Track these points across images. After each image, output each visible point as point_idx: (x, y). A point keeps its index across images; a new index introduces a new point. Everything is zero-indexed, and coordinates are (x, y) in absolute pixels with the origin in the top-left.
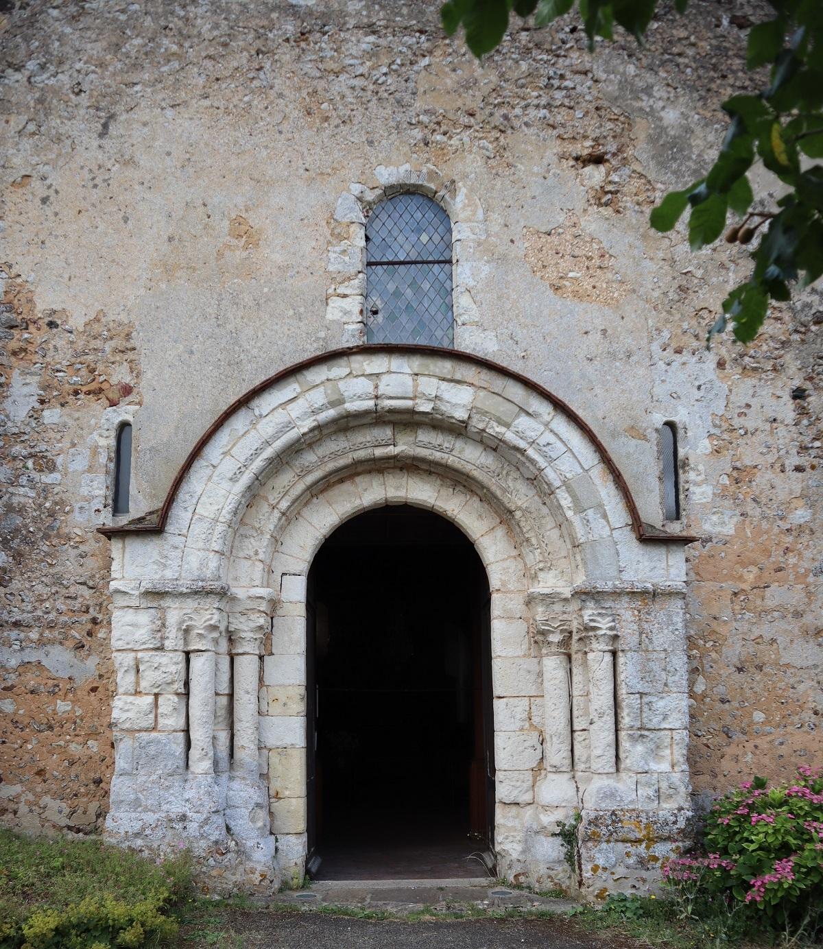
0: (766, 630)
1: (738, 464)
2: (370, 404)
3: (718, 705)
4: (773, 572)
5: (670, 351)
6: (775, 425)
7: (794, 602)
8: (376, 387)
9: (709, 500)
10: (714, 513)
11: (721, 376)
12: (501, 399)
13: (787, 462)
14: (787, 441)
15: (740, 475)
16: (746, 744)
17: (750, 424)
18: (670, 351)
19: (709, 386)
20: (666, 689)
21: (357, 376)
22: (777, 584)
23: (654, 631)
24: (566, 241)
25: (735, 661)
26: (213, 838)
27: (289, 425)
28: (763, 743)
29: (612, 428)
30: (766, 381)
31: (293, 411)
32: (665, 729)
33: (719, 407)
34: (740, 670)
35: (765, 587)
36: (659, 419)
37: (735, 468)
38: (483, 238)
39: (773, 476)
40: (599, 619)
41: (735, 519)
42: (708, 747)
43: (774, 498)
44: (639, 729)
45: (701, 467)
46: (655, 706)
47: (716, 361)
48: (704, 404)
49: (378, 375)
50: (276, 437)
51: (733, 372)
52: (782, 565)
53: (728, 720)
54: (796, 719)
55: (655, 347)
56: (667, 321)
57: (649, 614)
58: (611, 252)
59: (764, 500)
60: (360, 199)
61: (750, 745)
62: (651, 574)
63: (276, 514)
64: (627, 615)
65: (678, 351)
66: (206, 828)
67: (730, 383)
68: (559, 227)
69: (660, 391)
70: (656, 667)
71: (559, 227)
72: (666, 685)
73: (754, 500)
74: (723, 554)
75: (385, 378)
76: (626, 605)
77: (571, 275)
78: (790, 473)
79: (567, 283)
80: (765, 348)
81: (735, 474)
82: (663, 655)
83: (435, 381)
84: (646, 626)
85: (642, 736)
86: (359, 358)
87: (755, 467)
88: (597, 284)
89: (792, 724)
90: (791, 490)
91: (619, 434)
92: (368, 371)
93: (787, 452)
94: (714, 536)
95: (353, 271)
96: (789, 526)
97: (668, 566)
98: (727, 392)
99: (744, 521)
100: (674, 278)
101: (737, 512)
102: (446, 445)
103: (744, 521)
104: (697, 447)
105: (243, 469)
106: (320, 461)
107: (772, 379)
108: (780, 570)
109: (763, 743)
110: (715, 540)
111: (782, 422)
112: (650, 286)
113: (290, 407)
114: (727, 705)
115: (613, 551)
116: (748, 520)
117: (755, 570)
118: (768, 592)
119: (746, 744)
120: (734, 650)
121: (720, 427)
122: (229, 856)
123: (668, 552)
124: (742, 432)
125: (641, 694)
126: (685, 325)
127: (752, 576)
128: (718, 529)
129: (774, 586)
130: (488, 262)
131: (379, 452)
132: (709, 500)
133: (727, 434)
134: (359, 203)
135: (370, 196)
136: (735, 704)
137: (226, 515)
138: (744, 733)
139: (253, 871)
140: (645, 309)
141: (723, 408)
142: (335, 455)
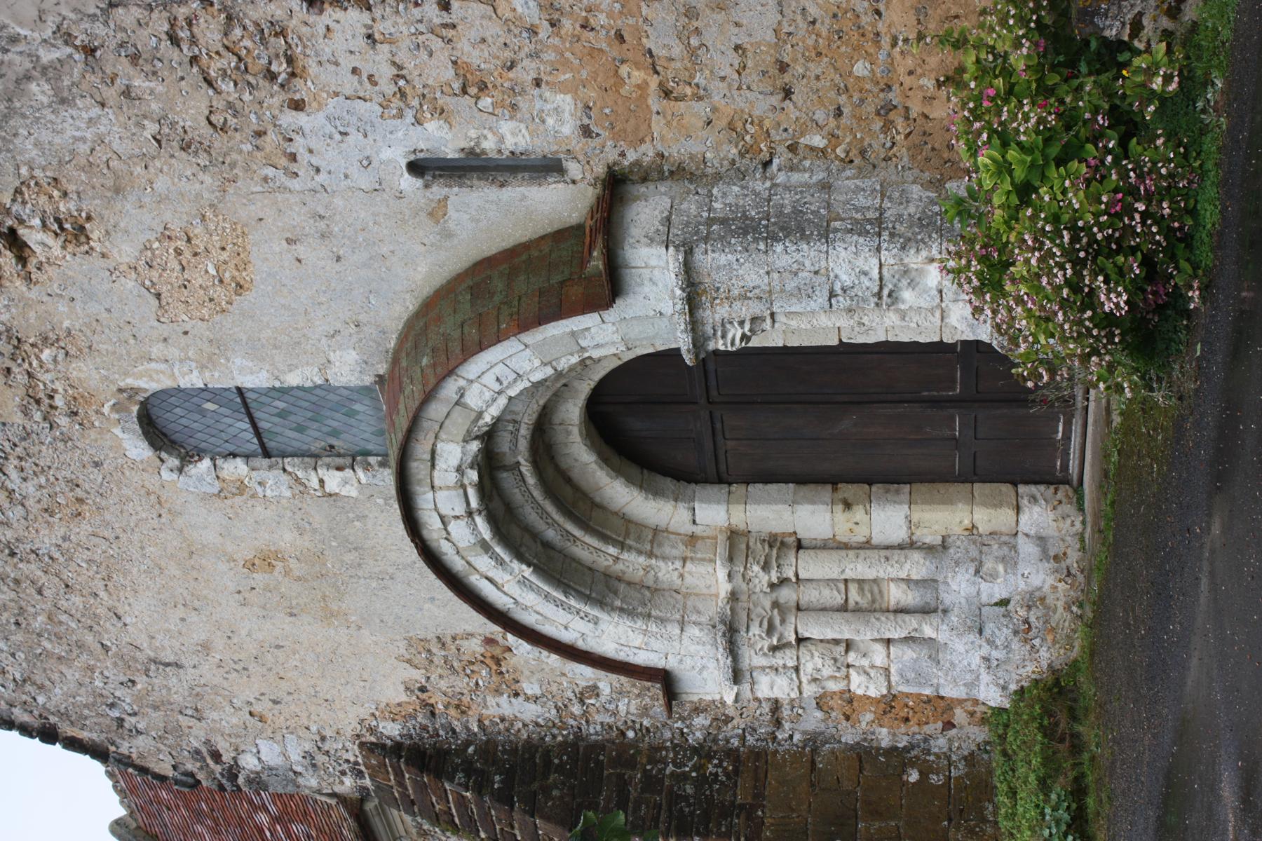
0: (725, 62)
1: (457, 86)
2: (480, 521)
3: (844, 120)
4: (625, 46)
5: (294, 167)
6: (377, 36)
7: (671, 19)
8: (457, 517)
9: (522, 126)
10: (543, 122)
11: (315, 104)
12: (447, 422)
13: (437, 21)
14: (400, 21)
15: (471, 84)
16: (906, 86)
17: (387, 71)
18: (294, 167)
19: (338, 123)
20: (823, 271)
21: (448, 533)
22: (644, 40)
23: (741, 284)
24: (161, 276)
25: (775, 100)
26: (1011, 636)
27: (523, 582)
28: (903, 65)
29: (438, 237)
30: (305, 47)
31: (511, 583)
32: (880, 273)
33: (370, 110)
34: (788, 93)
35: (652, 56)
36: (409, 183)
37: (464, 91)
38: (194, 364)
39: (464, 40)
40: (730, 336)
41: (547, 94)
42: (910, 133)
43: (502, 40)
44: (880, 298)
45: (473, 133)
46: (848, 283)
47: (294, 113)
48: (368, 128)
49: (442, 518)
50: (538, 591)
51: (302, 89)
52: (613, 32)
53: (870, 108)
54: (866, 20)
55: (295, 184)
56: (247, 169)
57: (718, 289)
58: (161, 229)
59: (508, 54)
60: (181, 470)
61: (908, 81)
62: (660, 285)
63: (625, 556)
64: (722, 311)
65: (293, 157)
66: (998, 642)
67: (325, 95)
68: (143, 285)
69: (364, 180)
70: (791, 285)
71: (143, 285)
72: (816, 273)
73: (510, 68)
74: (607, 111)
75: (445, 510)
76: (708, 312)
77: (212, 271)
78: (454, 16)
79: (227, 275)
80: (247, 43)
81: (473, 90)
82: (775, 276)
83: (436, 474)
84: (736, 292)
85: (890, 295)
86: (425, 533)
87: (455, 63)
88: (218, 246)
89: (874, 25)
90: (483, 17)
91: (444, 229)
92: (440, 525)
93: (421, 21)
94: (579, 123)
95: (285, 477)
96: (546, 24)
97: (646, 267)
98: (341, 98)
99: (547, 83)
100: (172, 156)
101: (536, 91)
102: (510, 428)
103: (547, 83)
104: (443, 139)
105: (582, 614)
106: (554, 526)
107: (300, 39)
108: (620, 37)
109: (903, 65)
110: (586, 121)
111: (371, 27)
112: (198, 186)
113: (500, 581)
114: (846, 111)
115: (635, 322)
116: (545, 78)
117: (624, 70)
118: (659, 52)
119: (906, 86)
120: (759, 103)
121: (401, 110)
122: (1032, 619)
123: (627, 267)
124: (402, 83)
125: (832, 294)
126: (247, 147)
127: (636, 73)
128: (567, 116)
129: (648, 43)
130: (228, 360)
131: (531, 481)
132: (522, 126)
133: (404, 96)
134: (186, 469)
135: (174, 462)
136: (843, 99)
137: (640, 623)
138: (889, 87)
139: (1054, 588)
140: (235, 193)
141: (368, 104)
142: (543, 513)
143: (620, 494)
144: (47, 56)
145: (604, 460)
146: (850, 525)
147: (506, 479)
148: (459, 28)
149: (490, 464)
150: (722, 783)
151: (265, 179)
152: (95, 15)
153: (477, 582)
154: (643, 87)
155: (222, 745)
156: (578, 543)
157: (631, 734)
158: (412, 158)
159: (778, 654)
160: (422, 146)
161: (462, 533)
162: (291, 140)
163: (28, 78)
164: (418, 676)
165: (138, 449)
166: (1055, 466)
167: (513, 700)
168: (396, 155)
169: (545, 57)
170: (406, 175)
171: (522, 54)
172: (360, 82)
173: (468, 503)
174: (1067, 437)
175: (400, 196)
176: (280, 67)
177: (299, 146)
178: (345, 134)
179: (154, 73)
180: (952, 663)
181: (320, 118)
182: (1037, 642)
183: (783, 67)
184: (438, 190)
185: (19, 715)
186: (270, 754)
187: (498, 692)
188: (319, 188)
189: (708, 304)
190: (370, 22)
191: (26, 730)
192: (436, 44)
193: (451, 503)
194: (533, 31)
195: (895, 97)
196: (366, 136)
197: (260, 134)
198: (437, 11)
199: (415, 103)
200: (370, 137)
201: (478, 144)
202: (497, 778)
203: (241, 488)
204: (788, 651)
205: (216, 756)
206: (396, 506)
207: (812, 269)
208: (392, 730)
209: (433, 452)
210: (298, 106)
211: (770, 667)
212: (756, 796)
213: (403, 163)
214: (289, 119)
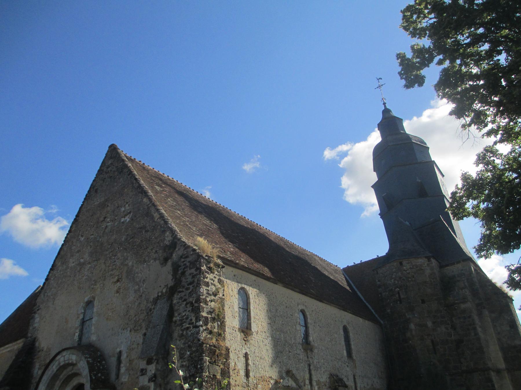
15: (131, 361)
104: (124, 357)
144: (141, 289)
145: (74, 387)
147: (71, 367)
149: (73, 365)
153: (54, 362)
155: (39, 311)
161: (61, 359)
163: (139, 286)
164: (45, 349)
165: (86, 299)
175: (116, 349)
176: (136, 328)
177: (125, 331)
181: (128, 335)
184: (116, 356)
185: (50, 275)
186: (37, 320)
187: (40, 365)
191: (48, 275)
202: (517, 233)
203: (78, 318)
205: (38, 310)
206: (11, 361)
208: (37, 344)
210: (130, 331)
214: (129, 329)
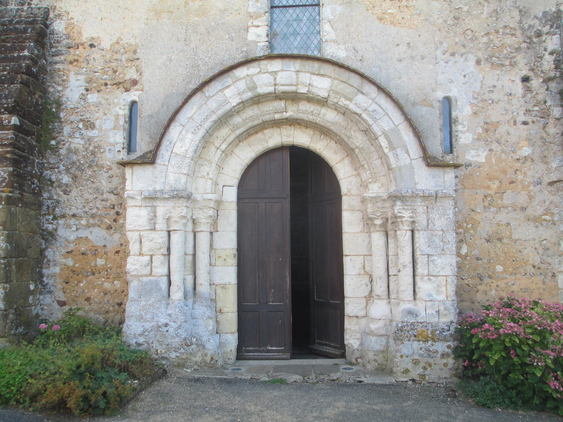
1: (488, 121)
4: (508, 184)
8: (275, 79)
13: (518, 120)
15: (489, 127)
16: (492, 284)
21: (264, 73)
34: (488, 241)
37: (486, 123)
40: (403, 211)
51: (486, 67)
55: (439, 52)
61: (494, 285)
63: (219, 152)
65: (453, 55)
66: (179, 331)
72: (443, 250)
77: (389, 11)
86: (265, 62)
87: (498, 122)
93: (518, 113)
108: (512, 182)
110: (473, 165)
112: (436, 17)
114: (480, 262)
117: (497, 183)
122: (192, 347)
124: (490, 102)
133: (481, 103)
143: (247, 154)
146: (224, 256)
148: (515, 127)
150: (31, 186)
151: (441, 43)
152: (516, 4)
154: (488, 187)
156: (230, 132)
157: (53, 142)
158: (453, 99)
159: (165, 221)
160: (459, 103)
162: (462, 56)
166: (248, 347)
167: (83, 88)
168: (453, 93)
169: (503, 155)
170: (444, 95)
171: (503, 147)
172: (489, 87)
173: (283, 85)
174: (269, 351)
178: (465, 76)
179: (491, 17)
180: (158, 308)
182: (182, 350)
183: (500, 240)
188: (437, 61)
189: (424, 204)
190: (517, 96)
192: (508, 117)
193: (282, 78)
194: (514, 152)
195: (486, 280)
196: (463, 84)
197: (464, 46)
198: (521, 120)
199: (480, 105)
200: (463, 85)
201: (460, 124)
204: (165, 225)
207: (445, 248)
209: (323, 75)
211: (155, 216)
212: (26, 203)
213: (450, 94)
